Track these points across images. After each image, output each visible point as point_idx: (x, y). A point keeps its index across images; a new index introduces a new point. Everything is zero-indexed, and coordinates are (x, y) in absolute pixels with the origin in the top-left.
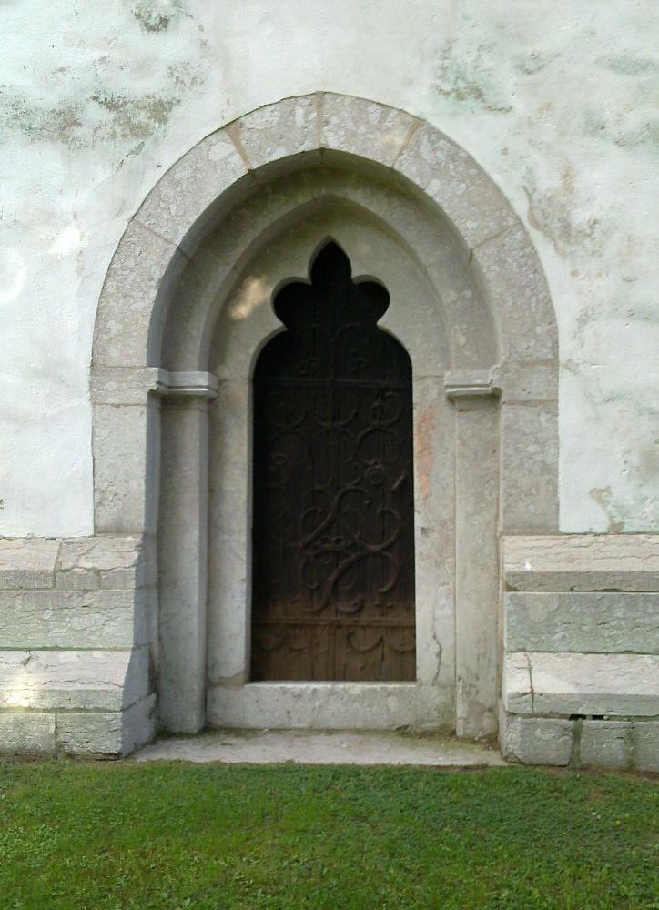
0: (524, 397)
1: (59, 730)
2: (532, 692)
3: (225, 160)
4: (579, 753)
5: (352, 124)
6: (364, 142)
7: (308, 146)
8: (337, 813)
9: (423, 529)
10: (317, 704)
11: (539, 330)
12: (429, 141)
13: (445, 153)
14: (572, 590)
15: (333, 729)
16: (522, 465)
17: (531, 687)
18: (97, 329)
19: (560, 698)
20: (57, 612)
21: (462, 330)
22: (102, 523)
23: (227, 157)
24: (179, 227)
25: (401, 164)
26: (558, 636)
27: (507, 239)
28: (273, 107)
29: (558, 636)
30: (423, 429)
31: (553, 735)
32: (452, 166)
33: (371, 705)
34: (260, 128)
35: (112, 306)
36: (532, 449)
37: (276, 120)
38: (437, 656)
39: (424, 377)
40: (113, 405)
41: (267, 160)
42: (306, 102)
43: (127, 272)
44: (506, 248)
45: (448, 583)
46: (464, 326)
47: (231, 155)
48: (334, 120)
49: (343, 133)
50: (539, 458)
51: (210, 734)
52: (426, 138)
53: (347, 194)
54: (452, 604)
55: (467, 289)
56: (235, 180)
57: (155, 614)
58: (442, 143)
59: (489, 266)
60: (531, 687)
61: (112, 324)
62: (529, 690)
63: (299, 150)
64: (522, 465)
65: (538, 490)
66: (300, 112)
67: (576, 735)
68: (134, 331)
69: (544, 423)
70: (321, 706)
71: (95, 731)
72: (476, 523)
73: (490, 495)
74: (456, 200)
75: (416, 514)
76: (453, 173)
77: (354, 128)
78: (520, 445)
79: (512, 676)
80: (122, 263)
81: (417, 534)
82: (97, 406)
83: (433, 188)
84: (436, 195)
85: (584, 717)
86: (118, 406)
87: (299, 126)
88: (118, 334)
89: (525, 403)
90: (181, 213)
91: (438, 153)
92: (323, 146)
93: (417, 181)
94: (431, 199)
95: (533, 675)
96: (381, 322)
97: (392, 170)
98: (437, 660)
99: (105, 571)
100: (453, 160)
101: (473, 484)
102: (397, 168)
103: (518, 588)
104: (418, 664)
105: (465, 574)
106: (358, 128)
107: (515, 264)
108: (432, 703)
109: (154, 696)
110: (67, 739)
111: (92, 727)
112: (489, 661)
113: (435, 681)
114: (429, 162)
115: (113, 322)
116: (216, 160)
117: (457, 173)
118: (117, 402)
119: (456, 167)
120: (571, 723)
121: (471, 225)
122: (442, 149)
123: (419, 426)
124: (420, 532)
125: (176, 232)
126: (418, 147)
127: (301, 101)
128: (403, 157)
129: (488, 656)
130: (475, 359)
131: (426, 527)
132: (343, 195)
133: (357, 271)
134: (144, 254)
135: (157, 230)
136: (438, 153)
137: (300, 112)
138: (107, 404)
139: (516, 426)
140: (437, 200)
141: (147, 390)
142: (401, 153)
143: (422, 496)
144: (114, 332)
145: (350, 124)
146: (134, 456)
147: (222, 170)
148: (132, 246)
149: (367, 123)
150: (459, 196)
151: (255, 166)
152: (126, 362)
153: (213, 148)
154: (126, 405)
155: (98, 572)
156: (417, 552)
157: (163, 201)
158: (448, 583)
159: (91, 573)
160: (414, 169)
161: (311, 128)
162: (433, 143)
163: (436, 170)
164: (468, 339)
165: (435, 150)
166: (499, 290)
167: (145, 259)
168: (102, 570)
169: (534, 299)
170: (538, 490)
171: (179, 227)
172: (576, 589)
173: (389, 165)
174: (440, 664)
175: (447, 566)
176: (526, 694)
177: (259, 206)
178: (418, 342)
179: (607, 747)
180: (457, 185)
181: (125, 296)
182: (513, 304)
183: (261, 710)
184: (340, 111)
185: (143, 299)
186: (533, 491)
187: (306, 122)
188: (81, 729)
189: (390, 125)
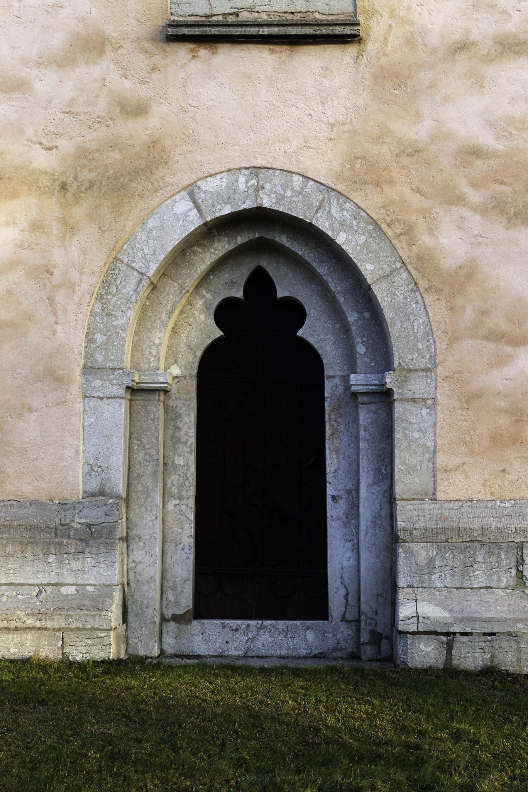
0: (410, 395)
1: (64, 644)
2: (418, 617)
3: (185, 214)
4: (451, 659)
5: (280, 189)
6: (289, 203)
7: (248, 205)
8: (390, 438)
9: (334, 498)
10: (250, 636)
11: (420, 346)
12: (338, 203)
13: (350, 213)
14: (446, 541)
15: (263, 656)
16: (409, 447)
17: (417, 612)
18: (87, 339)
19: (438, 623)
20: (59, 557)
21: (363, 342)
22: (89, 488)
23: (187, 212)
24: (150, 263)
25: (317, 220)
26: (437, 576)
27: (396, 278)
28: (222, 175)
29: (437, 576)
30: (333, 417)
31: (432, 647)
32: (355, 223)
33: (293, 638)
34: (212, 190)
35: (98, 322)
36: (416, 435)
37: (224, 184)
38: (344, 597)
39: (333, 377)
40: (98, 398)
41: (218, 215)
42: (247, 172)
43: (110, 297)
44: (395, 284)
45: (353, 540)
46: (364, 339)
47: (190, 210)
48: (268, 186)
49: (274, 196)
50: (422, 442)
51: (172, 654)
52: (335, 201)
53: (274, 238)
54: (356, 556)
55: (367, 311)
56: (193, 229)
57: (126, 560)
58: (348, 205)
59: (383, 297)
60: (417, 612)
61: (98, 336)
62: (415, 615)
63: (242, 208)
64: (409, 447)
65: (421, 466)
66: (242, 179)
67: (449, 647)
68: (115, 342)
69: (425, 416)
70: (253, 638)
71: (93, 645)
72: (375, 491)
73: (385, 470)
74: (358, 248)
75: (328, 484)
76: (355, 228)
77: (283, 193)
78: (408, 432)
79: (403, 605)
80: (106, 290)
81: (329, 500)
82: (86, 399)
83: (341, 239)
84: (344, 244)
85: (454, 634)
86: (102, 398)
87: (242, 190)
88: (103, 343)
89: (414, 401)
90: (152, 252)
91: (345, 213)
92: (259, 206)
93: (329, 233)
94: (340, 246)
95: (215, 13)
96: (299, 333)
97: (311, 224)
98: (344, 601)
99: (95, 525)
100: (356, 218)
101: (373, 461)
102: (314, 222)
103: (408, 540)
104: (330, 604)
105: (367, 533)
106: (285, 192)
107: (402, 296)
108: (341, 635)
109: (125, 625)
110: (72, 651)
111: (90, 642)
112: (386, 599)
113: (344, 619)
114: (338, 219)
115: (99, 334)
116: (179, 213)
117: (358, 228)
118: (101, 395)
119: (358, 223)
120: (444, 639)
121: (369, 267)
122: (347, 210)
123: (330, 415)
124: (331, 499)
125: (148, 267)
126: (330, 208)
127: (243, 171)
128: (319, 215)
129: (385, 596)
130: (373, 364)
131: (336, 495)
132: (272, 238)
133: (281, 293)
134: (123, 283)
135: (133, 265)
136: (345, 213)
137: (242, 179)
138: (94, 397)
139: (404, 418)
140: (344, 247)
141: (125, 386)
142: (317, 212)
143: (333, 470)
144: (99, 342)
145: (279, 189)
146: (114, 437)
147: (183, 221)
148: (114, 277)
149: (292, 189)
150: (360, 245)
151: (209, 219)
152: (109, 365)
153: (177, 204)
154: (108, 398)
155: (89, 526)
156: (328, 515)
157: (139, 244)
158: (353, 540)
159: (84, 527)
160: (327, 224)
161: (250, 191)
162: (340, 205)
163: (344, 226)
164: (367, 349)
165: (342, 210)
166: (391, 316)
167: (124, 287)
168: (93, 525)
169: (416, 322)
170: (421, 466)
171: (150, 263)
172: (450, 541)
173: (309, 221)
174: (347, 603)
175: (352, 526)
176: (412, 617)
177: (208, 244)
178: (329, 349)
179: (471, 657)
180: (359, 237)
181: (109, 315)
182: (401, 326)
183: (206, 640)
184: (272, 180)
185: (122, 317)
186: (418, 467)
187: (247, 187)
188: (81, 644)
189: (309, 190)
